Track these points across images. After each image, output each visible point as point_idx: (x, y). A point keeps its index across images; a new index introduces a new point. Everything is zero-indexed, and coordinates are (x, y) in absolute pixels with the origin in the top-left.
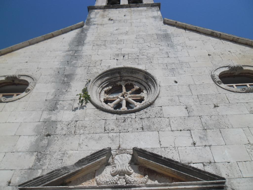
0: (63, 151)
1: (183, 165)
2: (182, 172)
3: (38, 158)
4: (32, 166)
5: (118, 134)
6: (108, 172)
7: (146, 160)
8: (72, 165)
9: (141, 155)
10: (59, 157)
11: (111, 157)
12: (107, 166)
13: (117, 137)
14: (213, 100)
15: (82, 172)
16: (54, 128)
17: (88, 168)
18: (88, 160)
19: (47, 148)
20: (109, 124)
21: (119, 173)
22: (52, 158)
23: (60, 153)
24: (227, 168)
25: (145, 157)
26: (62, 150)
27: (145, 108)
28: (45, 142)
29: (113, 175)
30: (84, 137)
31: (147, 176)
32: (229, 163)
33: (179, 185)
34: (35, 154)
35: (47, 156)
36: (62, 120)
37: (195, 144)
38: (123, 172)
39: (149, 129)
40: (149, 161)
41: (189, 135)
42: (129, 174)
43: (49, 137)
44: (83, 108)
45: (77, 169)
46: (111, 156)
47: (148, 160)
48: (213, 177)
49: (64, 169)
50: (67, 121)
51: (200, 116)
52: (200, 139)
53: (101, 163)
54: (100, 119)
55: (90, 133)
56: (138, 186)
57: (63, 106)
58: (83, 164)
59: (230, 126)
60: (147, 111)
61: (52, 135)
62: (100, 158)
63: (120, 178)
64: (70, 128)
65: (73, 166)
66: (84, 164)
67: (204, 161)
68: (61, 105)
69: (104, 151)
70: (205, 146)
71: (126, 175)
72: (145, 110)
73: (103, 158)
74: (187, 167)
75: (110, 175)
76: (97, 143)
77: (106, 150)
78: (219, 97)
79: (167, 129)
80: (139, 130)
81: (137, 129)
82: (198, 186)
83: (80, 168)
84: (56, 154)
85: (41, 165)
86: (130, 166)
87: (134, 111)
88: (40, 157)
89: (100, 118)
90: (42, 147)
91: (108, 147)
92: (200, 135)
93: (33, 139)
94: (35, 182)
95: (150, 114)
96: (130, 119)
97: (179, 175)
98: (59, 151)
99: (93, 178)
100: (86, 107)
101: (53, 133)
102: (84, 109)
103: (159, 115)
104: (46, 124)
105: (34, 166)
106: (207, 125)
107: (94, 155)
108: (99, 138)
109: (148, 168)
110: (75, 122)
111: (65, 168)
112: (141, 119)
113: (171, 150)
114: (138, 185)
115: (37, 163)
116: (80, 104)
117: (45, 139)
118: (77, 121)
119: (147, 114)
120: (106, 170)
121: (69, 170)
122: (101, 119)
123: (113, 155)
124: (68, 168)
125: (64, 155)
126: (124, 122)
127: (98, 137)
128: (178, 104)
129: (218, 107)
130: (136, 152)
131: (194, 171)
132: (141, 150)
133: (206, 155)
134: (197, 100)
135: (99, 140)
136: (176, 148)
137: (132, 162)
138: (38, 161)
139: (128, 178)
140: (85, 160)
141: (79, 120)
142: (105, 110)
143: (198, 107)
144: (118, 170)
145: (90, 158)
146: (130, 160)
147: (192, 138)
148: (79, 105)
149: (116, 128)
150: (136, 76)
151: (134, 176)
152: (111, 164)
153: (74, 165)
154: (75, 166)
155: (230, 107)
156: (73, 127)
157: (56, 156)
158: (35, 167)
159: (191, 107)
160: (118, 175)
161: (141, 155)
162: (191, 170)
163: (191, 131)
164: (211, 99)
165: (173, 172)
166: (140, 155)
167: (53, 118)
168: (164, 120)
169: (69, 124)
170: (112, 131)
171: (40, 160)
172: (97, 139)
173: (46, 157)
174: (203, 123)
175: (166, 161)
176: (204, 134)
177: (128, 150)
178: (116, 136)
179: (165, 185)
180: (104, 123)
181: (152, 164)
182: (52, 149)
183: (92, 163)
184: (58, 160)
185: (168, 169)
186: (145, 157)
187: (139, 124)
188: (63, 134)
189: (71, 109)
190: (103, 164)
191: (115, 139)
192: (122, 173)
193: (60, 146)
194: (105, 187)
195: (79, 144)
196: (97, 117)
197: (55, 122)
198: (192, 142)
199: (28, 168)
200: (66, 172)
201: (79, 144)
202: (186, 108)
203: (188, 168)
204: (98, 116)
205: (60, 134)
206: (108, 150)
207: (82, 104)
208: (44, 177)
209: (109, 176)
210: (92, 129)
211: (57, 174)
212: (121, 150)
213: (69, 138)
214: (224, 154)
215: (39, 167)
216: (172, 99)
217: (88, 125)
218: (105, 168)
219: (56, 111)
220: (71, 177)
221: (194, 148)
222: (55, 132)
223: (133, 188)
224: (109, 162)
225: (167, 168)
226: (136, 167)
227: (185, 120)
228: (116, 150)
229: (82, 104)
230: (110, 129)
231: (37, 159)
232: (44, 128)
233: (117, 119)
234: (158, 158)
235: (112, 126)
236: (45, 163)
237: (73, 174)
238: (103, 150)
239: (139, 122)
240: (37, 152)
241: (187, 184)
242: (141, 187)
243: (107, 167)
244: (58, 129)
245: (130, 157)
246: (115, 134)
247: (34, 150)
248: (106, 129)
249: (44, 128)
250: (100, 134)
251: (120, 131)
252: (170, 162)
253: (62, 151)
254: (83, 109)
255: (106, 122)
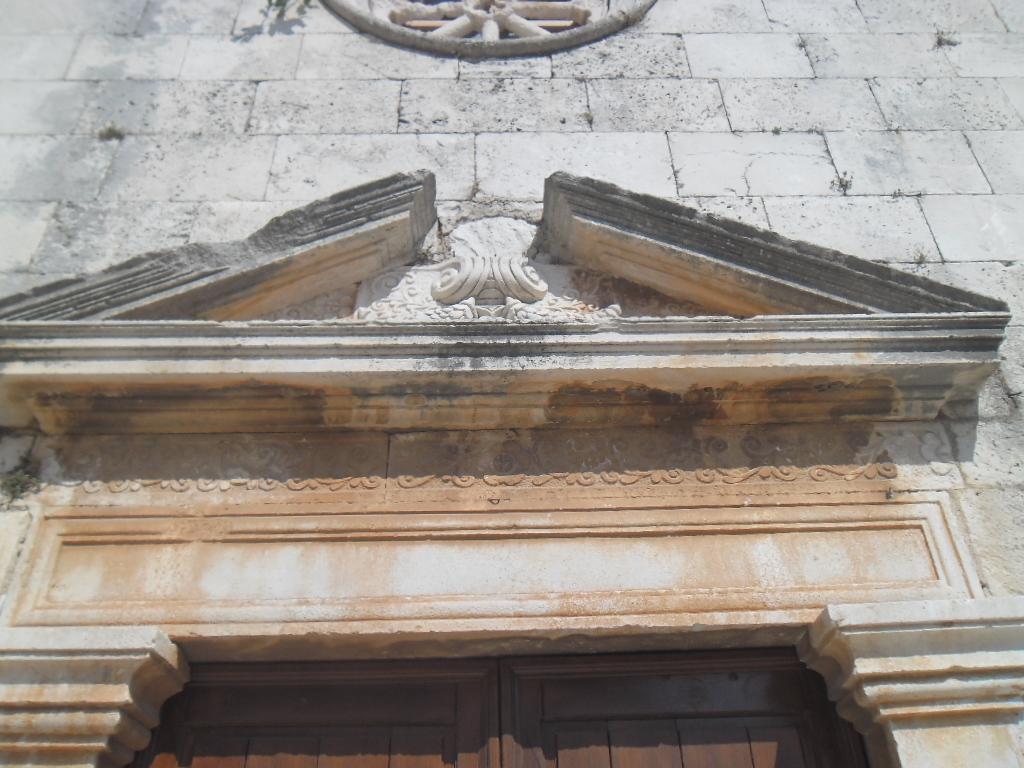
0: (189, 201)
2: (790, 284)
3: (59, 228)
4: (32, 261)
5: (466, 138)
7: (617, 235)
11: (434, 230)
12: (414, 268)
15: (291, 282)
17: (318, 263)
18: (321, 221)
21: (476, 292)
22: (130, 227)
24: (999, 286)
25: (610, 218)
26: (181, 198)
27: (598, 40)
29: (445, 301)
32: (1009, 264)
33: (784, 328)
34: (51, 208)
36: (179, 76)
37: (844, 186)
38: (498, 288)
40: (627, 237)
41: (820, 151)
43: (114, 142)
45: (263, 260)
48: (949, 300)
49: (193, 256)
52: (873, 166)
53: (383, 247)
54: (374, 75)
55: (323, 130)
56: (575, 327)
60: (607, 50)
62: (380, 218)
63: (479, 311)
65: (244, 246)
66: (297, 237)
67: (891, 256)
69: (398, 185)
70: (896, 195)
71: (510, 300)
72: (601, 46)
73: (398, 217)
74: (818, 259)
76: (360, 173)
77: (412, 182)
79: (709, 125)
80: (567, 127)
82: (877, 332)
83: (277, 258)
84: (156, 211)
85: (75, 255)
86: (528, 264)
87: (547, 48)
90: (82, 182)
91: (420, 169)
92: (870, 153)
93: (35, 150)
94: (42, 304)
95: (624, 61)
96: (527, 80)
97: (773, 302)
99: (348, 315)
100: (302, 25)
101: (136, 128)
103: (669, 70)
104: (99, 90)
105: (41, 260)
106: (902, 114)
108: (371, 153)
109: (616, 277)
110: (248, 88)
111: (200, 251)
112: (581, 80)
114: (580, 324)
116: (273, 14)
117: (94, 149)
118: (257, 82)
122: (381, 77)
123: (443, 221)
124: (217, 255)
128: (760, 27)
131: (854, 275)
132: (586, 187)
135: (371, 161)
136: (756, 201)
137: (538, 252)
138: (60, 241)
139: (521, 309)
140: (305, 219)
141: (270, 77)
142: (400, 39)
145: (329, 212)
146: (530, 244)
147: (833, 164)
148: (266, 15)
152: (436, 258)
153: (247, 243)
156: (240, 103)
158: (46, 263)
159: (827, 43)
160: (471, 300)
162: (837, 270)
163: (827, 134)
165: (747, 285)
166: (581, 209)
167: (136, 65)
170: (434, 127)
171: (69, 237)
172: (363, 157)
173: (101, 222)
174: (882, 107)
176: (888, 148)
177: (520, 205)
178: (459, 148)
179: (712, 326)
181: (642, 253)
182: (132, 190)
183: (339, 237)
184: (164, 239)
185: (721, 271)
187: (569, 100)
188: (186, 133)
189: (227, 32)
191: (451, 159)
192: (492, 293)
194: (409, 329)
195: (271, 174)
197: (142, 81)
199: (11, 266)
200: (208, 269)
201: (271, 174)
202: (802, 45)
205: (174, 133)
206: (419, 183)
207: (281, 15)
208: (87, 285)
209: (427, 304)
210: (337, 115)
212: (480, 205)
213: (217, 149)
214: (984, 228)
215: (68, 264)
217: (314, 99)
219: (148, 37)
220: (235, 300)
221: (843, 201)
222: (147, 125)
223: (551, 334)
227: (796, 90)
228: (460, 201)
229: (281, 15)
230: (428, 116)
231: (55, 231)
232: (86, 105)
233: (458, 78)
234: (677, 222)
236: (99, 248)
237: (244, 288)
239: (569, 92)
240: (54, 205)
242: (596, 333)
243: (416, 271)
244: (159, 111)
245: (529, 233)
247: (41, 195)
248: (406, 118)
250: (377, 137)
251: (475, 125)
252: (736, 235)
254: (290, 32)
255: (405, 89)
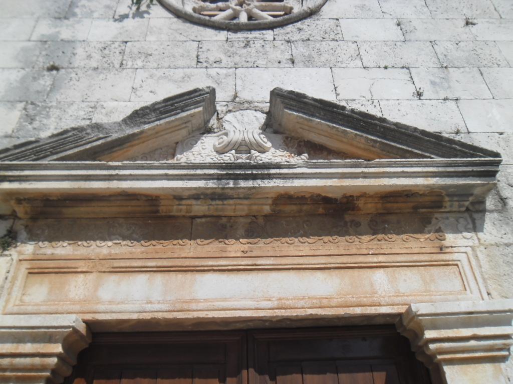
1: (397, 127)
2: (393, 144)
3: (27, 115)
4: (13, 131)
6: (207, 146)
7: (306, 119)
8: (115, 123)
9: (292, 107)
10: (83, 113)
11: (215, 117)
13: (230, 77)
14: (461, 10)
15: (143, 142)
16: (69, 54)
19: (50, 94)
20: (209, 50)
21: (236, 147)
22: (63, 115)
23: (84, 105)
25: (303, 111)
27: (297, 21)
30: (146, 75)
31: (306, 155)
32: (501, 134)
34: (22, 105)
35: (51, 110)
37: (420, 95)
38: (247, 146)
40: (311, 120)
43: (54, 72)
44: (143, 16)
45: (130, 131)
46: (214, 113)
47: (310, 118)
50: (101, 40)
51: (431, 42)
52: (433, 85)
53: (189, 125)
54: (185, 39)
57: (90, 9)
58: (145, 122)
59: (503, 63)
60: (301, 27)
61: (63, 68)
64: (109, 57)
65: (119, 124)
66: (146, 120)
68: (86, 8)
69: (197, 94)
70: (445, 99)
71: (253, 152)
72: (298, 25)
73: (197, 110)
74: (407, 131)
75: (212, 152)
76: (178, 88)
77: (204, 92)
78: (477, 6)
79: (352, 64)
80: (282, 65)
81: (280, 62)
83: (136, 130)
84: (75, 107)
85: (34, 129)
86: (262, 134)
88: (32, 112)
89: (185, 37)
90: (38, 92)
91: (208, 86)
92: (433, 79)
93: (15, 76)
94: (18, 153)
95: (310, 32)
98: (83, 101)
100: (149, 13)
101: (65, 65)
102: (144, 17)
103: (332, 37)
104: (47, 46)
105: (18, 131)
107: (171, 102)
110: (122, 45)
111: (97, 127)
112: (288, 42)
113: (362, 105)
115: (26, 125)
116: (134, 8)
117: (44, 75)
118: (126, 42)
119: (301, 33)
120: (202, 143)
121: (107, 133)
122: (188, 39)
123: (219, 112)
124: (106, 129)
125: (94, 110)
126: (245, 46)
127: (182, 75)
128: (378, 16)
129: (474, 24)
130: (278, 100)
131: (424, 139)
132: (291, 95)
134: (423, 10)
138: (26, 122)
140: (150, 111)
141: (133, 40)
142: (197, 21)
143: (426, 23)
144: (235, 139)
146: (263, 123)
147: (414, 84)
148: (131, 8)
149: (225, 59)
151: (274, 155)
152: (216, 130)
154: (122, 125)
155: (503, 25)
156: (118, 52)
157: (73, 112)
158: (20, 133)
159: (411, 23)
160: (233, 152)
161: (292, 107)
162: (416, 137)
163: (411, 69)
164: (456, 9)
165: (371, 144)
166: (288, 106)
168: (345, 46)
169: (107, 48)
170: (215, 65)
171: (32, 120)
172: (179, 80)
173: (48, 112)
175: (354, 118)
176: (441, 76)
178: (227, 75)
180: (196, 49)
181: (320, 129)
182: (63, 96)
183: (167, 120)
186: (303, 111)
187: (282, 52)
189: (111, 17)
190: (195, 130)
191: (223, 81)
193: (84, 91)
195: (133, 88)
196: (178, 35)
197: (68, 42)
198: (412, 89)
200: (101, 136)
201: (133, 88)
202: (399, 25)
203: (411, 133)
204: (181, 34)
205: (84, 67)
207: (138, 9)
211: (77, 140)
212: (238, 104)
213: (106, 76)
215: (31, 133)
216: (365, 5)
217: (155, 51)
218: (199, 139)
221: (419, 102)
223: (273, 168)
224: (210, 125)
225: (356, 134)
226: (279, 138)
228: (228, 102)
229: (138, 9)
230: (212, 59)
231: (24, 116)
233: (227, 41)
234: (336, 112)
237: (120, 145)
238: (195, 91)
239: (282, 47)
240: (24, 103)
241: (409, 164)
244: (77, 56)
245: (262, 118)
246: (224, 71)
248: (201, 60)
249: (40, 53)
251: (235, 64)
252: (365, 120)
253: (88, 102)
255: (200, 46)
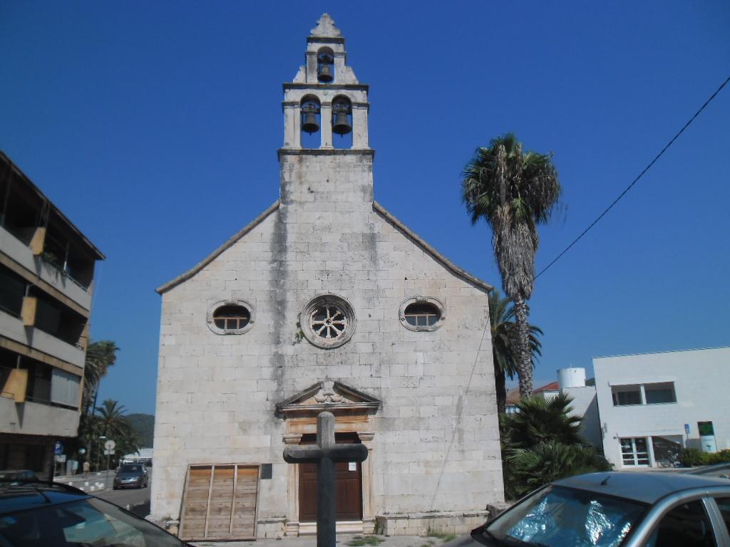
28: (280, 372)
39: (346, 363)
42: (333, 395)
72: (344, 346)
133: (377, 382)
150: (339, 302)
235: (322, 360)
